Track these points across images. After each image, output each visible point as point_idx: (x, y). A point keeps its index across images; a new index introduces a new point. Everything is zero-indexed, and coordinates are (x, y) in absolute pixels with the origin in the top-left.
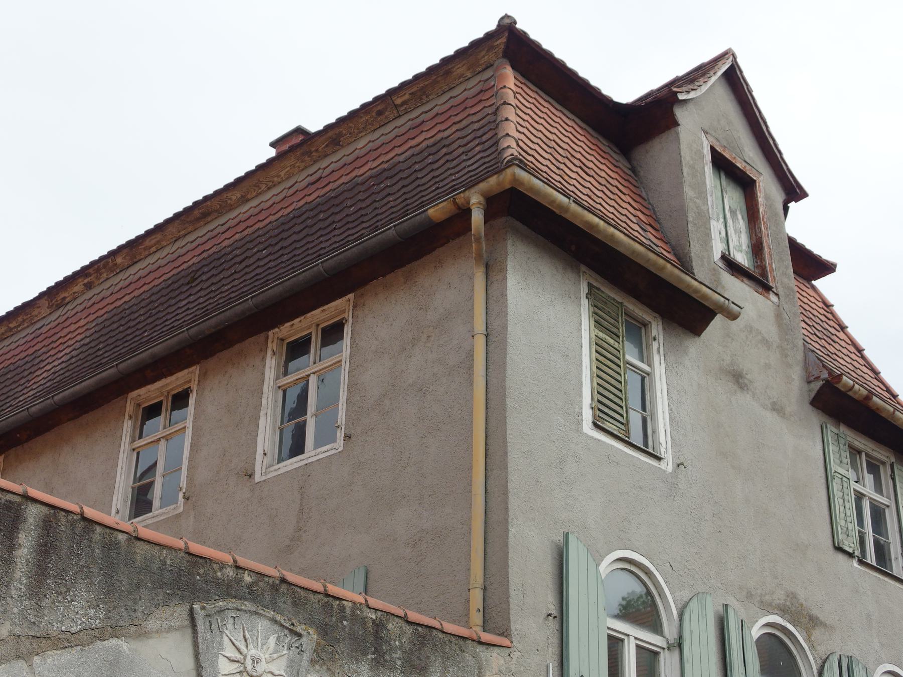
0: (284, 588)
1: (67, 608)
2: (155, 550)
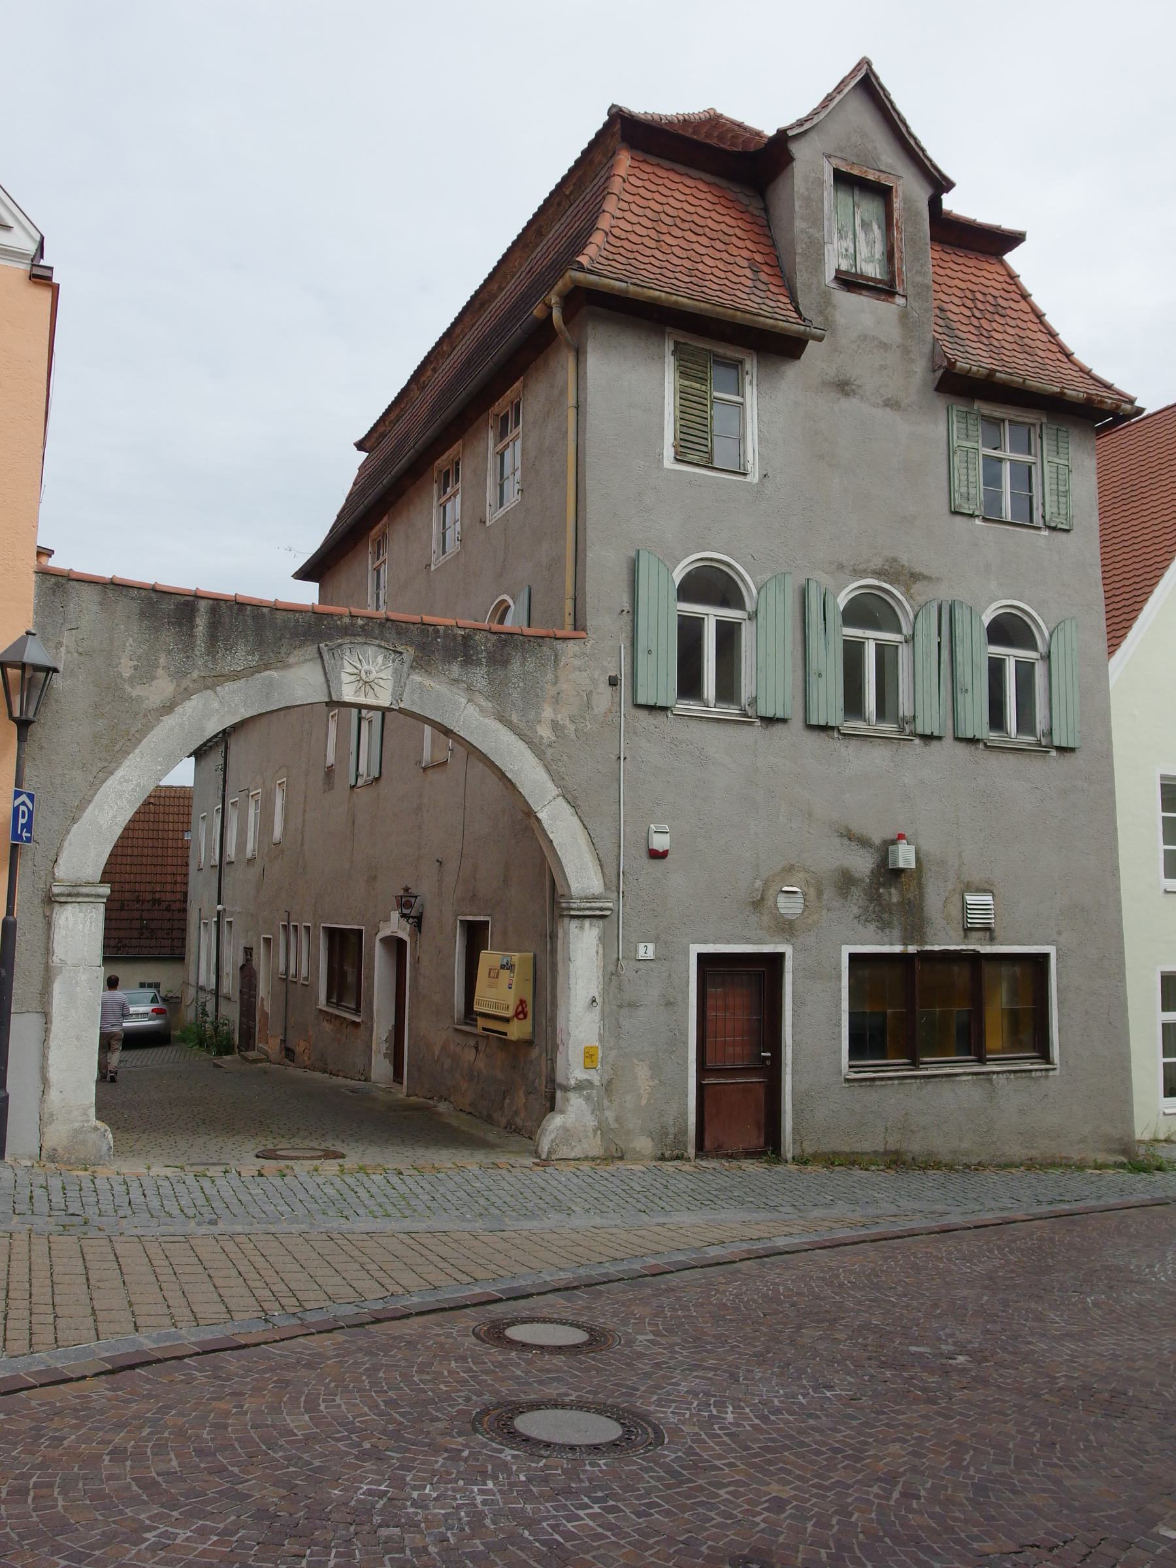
0: (389, 624)
1: (233, 658)
2: (291, 615)
